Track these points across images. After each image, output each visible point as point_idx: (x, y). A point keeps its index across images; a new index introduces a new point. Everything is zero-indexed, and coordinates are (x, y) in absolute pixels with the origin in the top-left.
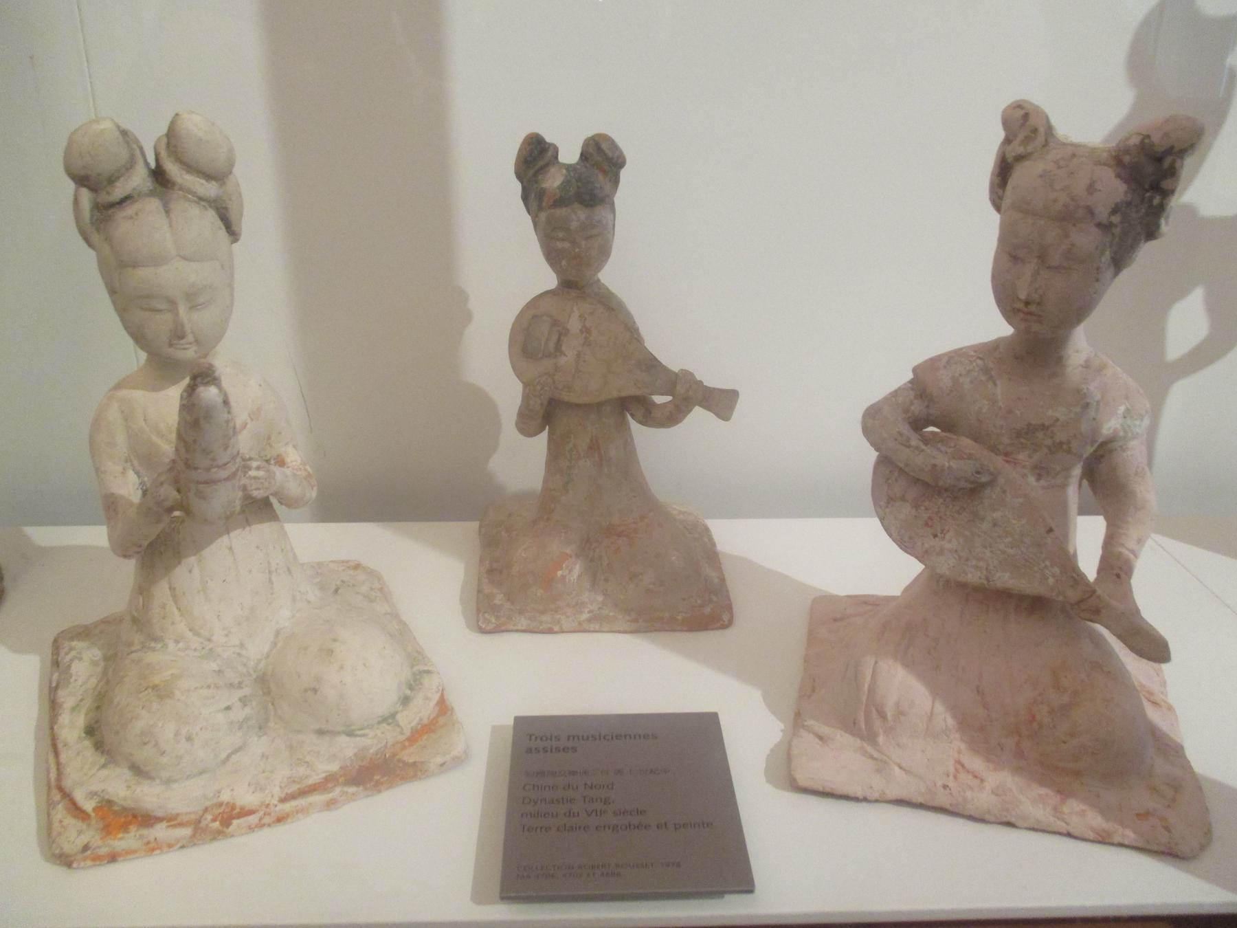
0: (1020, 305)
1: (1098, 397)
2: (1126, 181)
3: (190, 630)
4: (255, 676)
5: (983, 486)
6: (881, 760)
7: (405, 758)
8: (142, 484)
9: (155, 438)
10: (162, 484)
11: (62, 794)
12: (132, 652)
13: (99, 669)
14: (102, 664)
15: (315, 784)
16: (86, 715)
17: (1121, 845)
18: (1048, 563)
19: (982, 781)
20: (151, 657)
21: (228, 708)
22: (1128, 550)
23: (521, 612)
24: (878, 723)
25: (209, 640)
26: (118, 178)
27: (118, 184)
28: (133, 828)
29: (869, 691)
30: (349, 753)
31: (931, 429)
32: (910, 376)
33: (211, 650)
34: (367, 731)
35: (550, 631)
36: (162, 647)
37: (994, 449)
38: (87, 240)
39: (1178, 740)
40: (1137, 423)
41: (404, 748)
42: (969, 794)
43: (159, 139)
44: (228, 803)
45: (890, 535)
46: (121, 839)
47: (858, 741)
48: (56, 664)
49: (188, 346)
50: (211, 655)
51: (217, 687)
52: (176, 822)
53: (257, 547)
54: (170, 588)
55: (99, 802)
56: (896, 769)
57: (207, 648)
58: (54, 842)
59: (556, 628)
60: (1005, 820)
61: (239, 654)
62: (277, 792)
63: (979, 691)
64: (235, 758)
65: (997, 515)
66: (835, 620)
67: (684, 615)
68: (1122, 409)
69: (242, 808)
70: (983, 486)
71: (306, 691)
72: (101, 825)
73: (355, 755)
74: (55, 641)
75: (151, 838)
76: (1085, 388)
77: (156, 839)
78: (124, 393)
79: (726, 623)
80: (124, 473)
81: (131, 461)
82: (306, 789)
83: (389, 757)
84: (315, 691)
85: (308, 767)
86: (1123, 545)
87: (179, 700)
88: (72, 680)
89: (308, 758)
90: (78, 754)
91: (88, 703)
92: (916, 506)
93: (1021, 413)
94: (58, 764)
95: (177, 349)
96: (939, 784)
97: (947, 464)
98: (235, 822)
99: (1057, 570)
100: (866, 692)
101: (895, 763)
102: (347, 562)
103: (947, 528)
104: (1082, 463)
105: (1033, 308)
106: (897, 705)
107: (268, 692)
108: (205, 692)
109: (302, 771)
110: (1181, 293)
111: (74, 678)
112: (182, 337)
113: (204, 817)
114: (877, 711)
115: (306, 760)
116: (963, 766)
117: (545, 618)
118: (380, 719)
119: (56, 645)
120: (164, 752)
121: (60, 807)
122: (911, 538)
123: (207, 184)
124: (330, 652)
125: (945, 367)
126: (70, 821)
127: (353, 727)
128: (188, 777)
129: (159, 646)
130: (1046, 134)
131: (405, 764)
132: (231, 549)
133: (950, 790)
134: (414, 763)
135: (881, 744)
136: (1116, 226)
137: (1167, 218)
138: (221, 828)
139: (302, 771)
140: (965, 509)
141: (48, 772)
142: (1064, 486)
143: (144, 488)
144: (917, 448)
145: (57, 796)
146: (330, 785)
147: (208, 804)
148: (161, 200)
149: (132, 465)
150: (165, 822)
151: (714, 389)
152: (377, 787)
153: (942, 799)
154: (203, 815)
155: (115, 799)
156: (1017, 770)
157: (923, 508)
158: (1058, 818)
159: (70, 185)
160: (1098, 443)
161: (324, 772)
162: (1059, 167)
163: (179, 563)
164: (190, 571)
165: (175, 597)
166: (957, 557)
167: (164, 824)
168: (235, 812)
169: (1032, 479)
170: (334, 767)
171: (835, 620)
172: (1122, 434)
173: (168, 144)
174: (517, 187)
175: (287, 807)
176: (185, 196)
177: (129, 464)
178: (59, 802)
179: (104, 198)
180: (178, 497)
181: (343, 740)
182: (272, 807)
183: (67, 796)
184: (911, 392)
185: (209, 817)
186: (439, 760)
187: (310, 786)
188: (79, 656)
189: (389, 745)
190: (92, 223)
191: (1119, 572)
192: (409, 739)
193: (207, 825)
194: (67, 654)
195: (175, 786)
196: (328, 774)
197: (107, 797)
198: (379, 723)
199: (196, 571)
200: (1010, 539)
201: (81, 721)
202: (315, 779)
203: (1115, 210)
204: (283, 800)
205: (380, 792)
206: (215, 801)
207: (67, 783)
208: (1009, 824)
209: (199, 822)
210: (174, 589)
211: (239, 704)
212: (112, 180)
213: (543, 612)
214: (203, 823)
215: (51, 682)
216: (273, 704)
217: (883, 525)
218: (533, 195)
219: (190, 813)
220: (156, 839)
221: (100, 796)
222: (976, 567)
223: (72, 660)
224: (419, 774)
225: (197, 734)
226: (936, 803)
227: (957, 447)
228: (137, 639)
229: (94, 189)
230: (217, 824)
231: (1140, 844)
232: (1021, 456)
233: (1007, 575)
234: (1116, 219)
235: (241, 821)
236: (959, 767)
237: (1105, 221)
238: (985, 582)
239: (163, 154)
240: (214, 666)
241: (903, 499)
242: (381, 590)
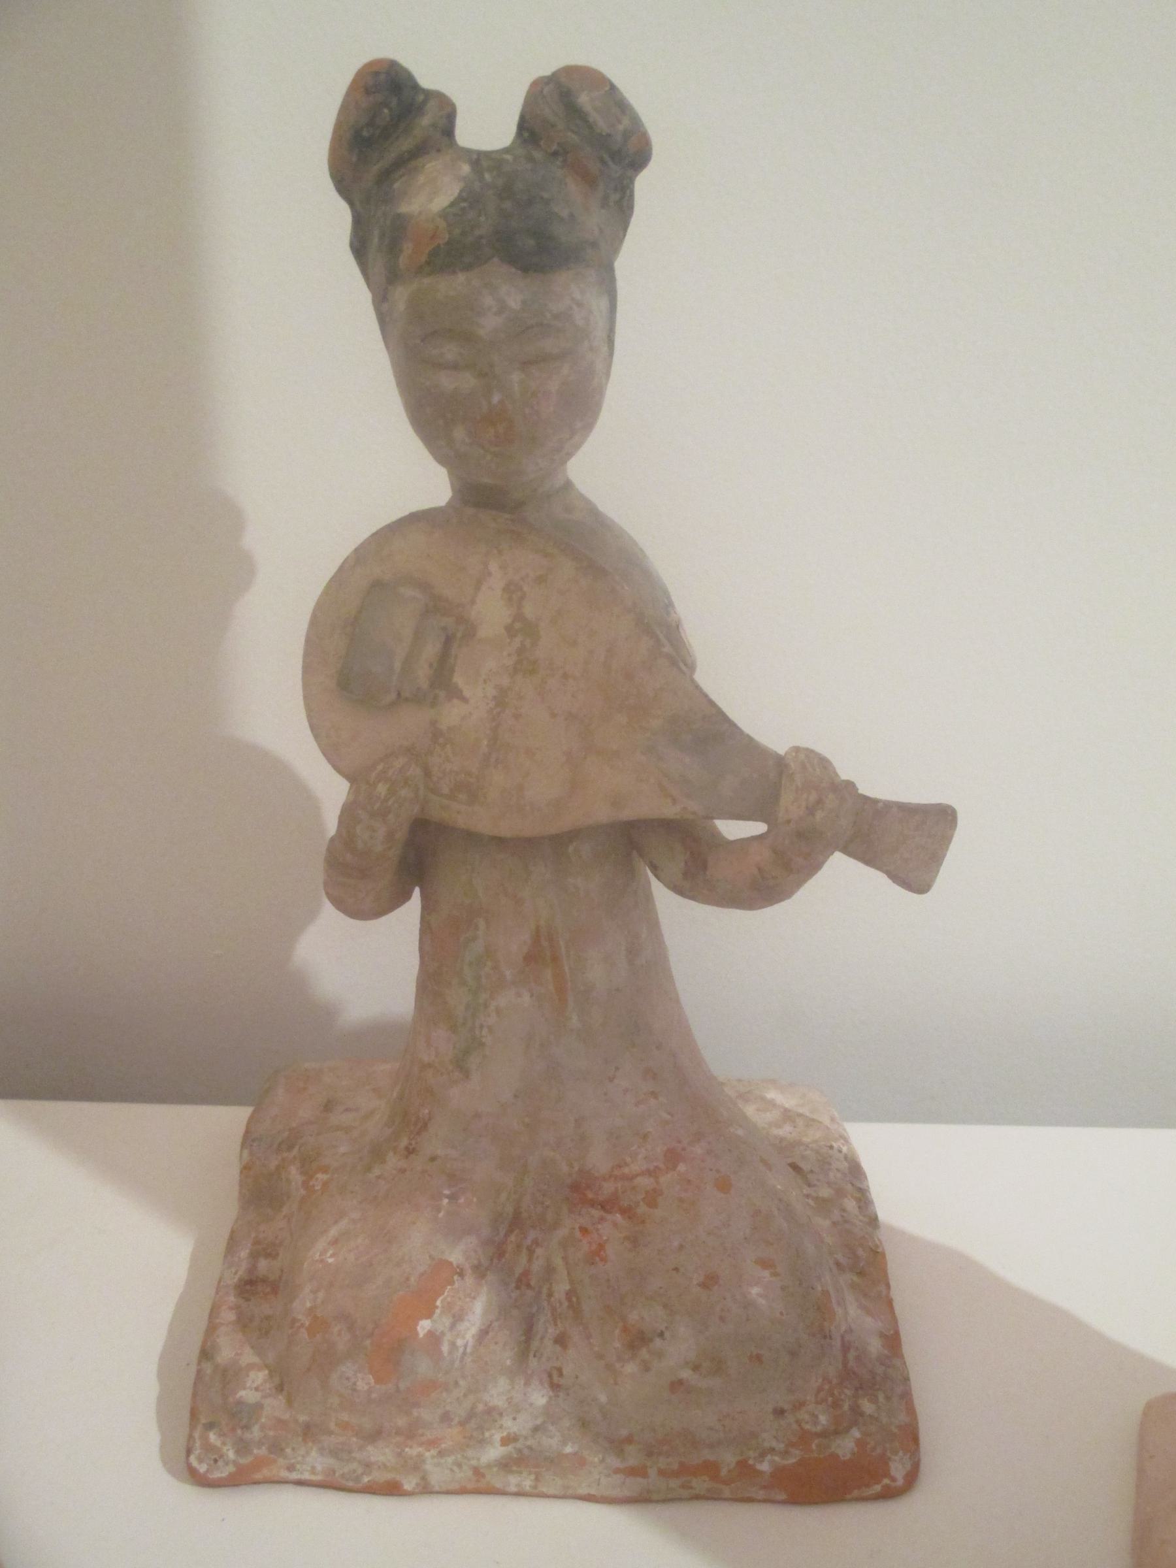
35: (392, 1489)
79: (900, 1482)
151: (889, 805)
213: (375, 1436)
231: (626, 1493)
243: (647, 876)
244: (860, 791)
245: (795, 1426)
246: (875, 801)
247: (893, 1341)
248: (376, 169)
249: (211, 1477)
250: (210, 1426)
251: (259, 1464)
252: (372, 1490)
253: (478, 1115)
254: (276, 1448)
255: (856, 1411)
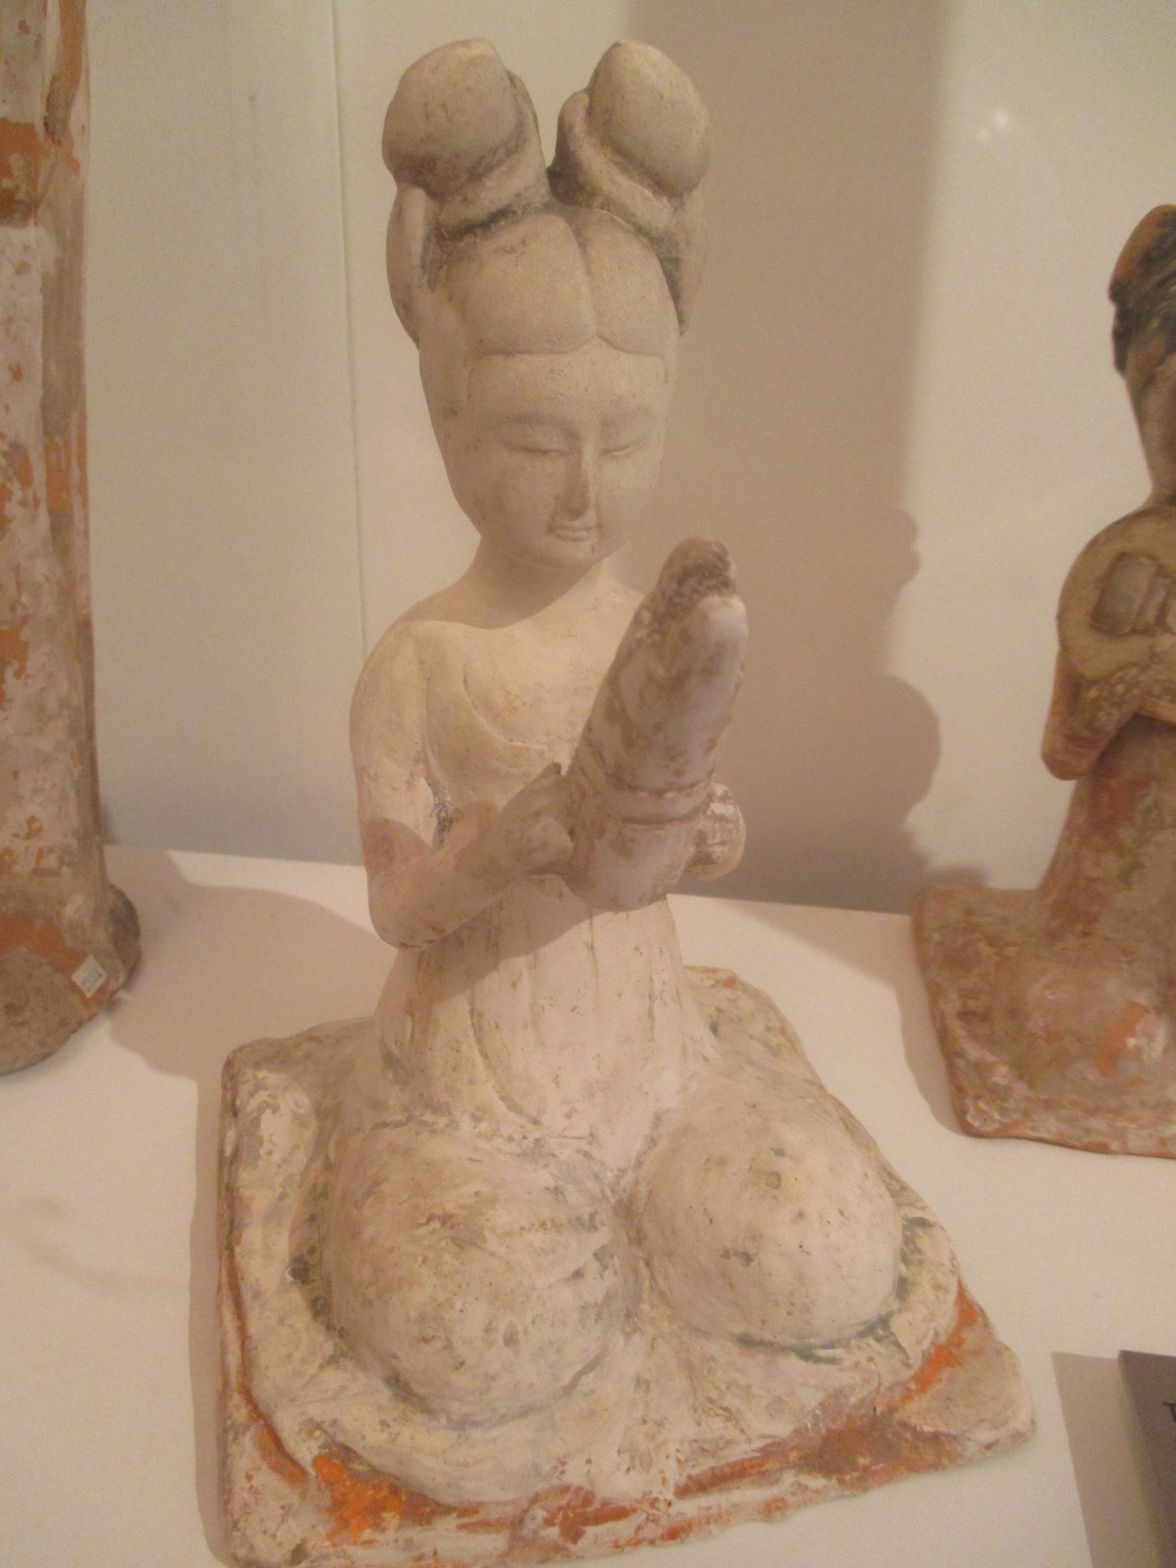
3: (502, 1098)
4: (613, 1200)
7: (914, 1421)
8: (441, 805)
9: (482, 721)
10: (537, 814)
11: (250, 1407)
12: (385, 1125)
13: (309, 1134)
14: (313, 1124)
15: (742, 1462)
16: (292, 1232)
20: (434, 1148)
21: (578, 1274)
23: (1049, 1105)
25: (536, 1122)
26: (490, 168)
27: (488, 182)
28: (391, 1518)
30: (811, 1399)
33: (537, 1141)
34: (838, 1352)
35: (1101, 1149)
36: (447, 1126)
38: (405, 308)
41: (907, 1397)
43: (573, 98)
44: (579, 1489)
46: (369, 1543)
48: (232, 1110)
49: (584, 534)
50: (537, 1152)
51: (558, 1227)
52: (474, 1519)
53: (637, 949)
54: (472, 1013)
55: (323, 1447)
57: (531, 1138)
58: (235, 1524)
59: (1115, 1145)
61: (587, 1155)
62: (676, 1476)
64: (588, 1381)
69: (605, 1503)
71: (726, 1254)
72: (327, 1501)
73: (822, 1405)
74: (229, 1064)
75: (427, 1550)
77: (435, 1553)
78: (429, 626)
80: (410, 784)
81: (426, 761)
82: (727, 1470)
83: (882, 1412)
84: (747, 1258)
85: (728, 1419)
87: (492, 1254)
88: (263, 1151)
89: (730, 1401)
90: (281, 1321)
91: (294, 1206)
94: (242, 1331)
95: (559, 537)
98: (590, 1531)
102: (715, 971)
107: (639, 1239)
108: (538, 1238)
109: (717, 1427)
111: (266, 1146)
112: (577, 513)
113: (530, 1514)
115: (725, 1404)
117: (1097, 1123)
118: (862, 1328)
119: (231, 1073)
120: (462, 1364)
121: (247, 1440)
123: (654, 199)
124: (775, 1180)
126: (266, 1478)
127: (812, 1341)
128: (503, 1420)
129: (442, 1122)
131: (918, 1435)
132: (591, 947)
134: (936, 1438)
138: (561, 1542)
139: (717, 1427)
141: (224, 1353)
143: (443, 814)
145: (241, 1413)
146: (770, 1465)
147: (541, 1486)
148: (570, 222)
149: (428, 768)
150: (454, 1515)
152: (863, 1481)
154: (530, 1507)
155: (358, 1447)
159: (387, 186)
161: (763, 1436)
163: (496, 966)
164: (514, 985)
165: (479, 1031)
167: (452, 1521)
168: (590, 1509)
170: (782, 1429)
173: (590, 112)
174: (1106, 314)
175: (690, 1507)
176: (613, 220)
177: (421, 766)
178: (247, 1428)
179: (457, 212)
180: (568, 843)
181: (792, 1364)
182: (662, 1505)
183: (261, 1417)
185: (540, 1514)
186: (985, 1435)
187: (732, 1465)
188: (271, 1101)
189: (882, 1389)
190: (423, 266)
192: (916, 1378)
193: (535, 1532)
194: (252, 1095)
195: (476, 1435)
196: (769, 1441)
197: (340, 1438)
198: (861, 1335)
199: (525, 984)
201: (283, 1245)
202: (741, 1451)
204: (683, 1492)
205: (865, 1490)
206: (556, 1482)
207: (264, 1389)
209: (521, 1522)
210: (480, 1015)
211: (595, 1265)
212: (478, 173)
213: (1093, 1112)
214: (526, 1532)
215: (222, 1151)
216: (648, 1264)
218: (1155, 323)
219: (506, 1503)
220: (435, 1553)
221: (326, 1433)
223: (261, 1109)
224: (945, 1460)
225: (526, 1332)
228: (394, 1096)
229: (436, 194)
230: (554, 1532)
235: (603, 1529)
239: (579, 126)
240: (545, 1178)
242: (783, 1031)
248: (1157, 278)
249: (982, 1129)
250: (977, 1097)
251: (1016, 1124)
252: (1088, 1148)
253: (1135, 913)
254: (1026, 1114)
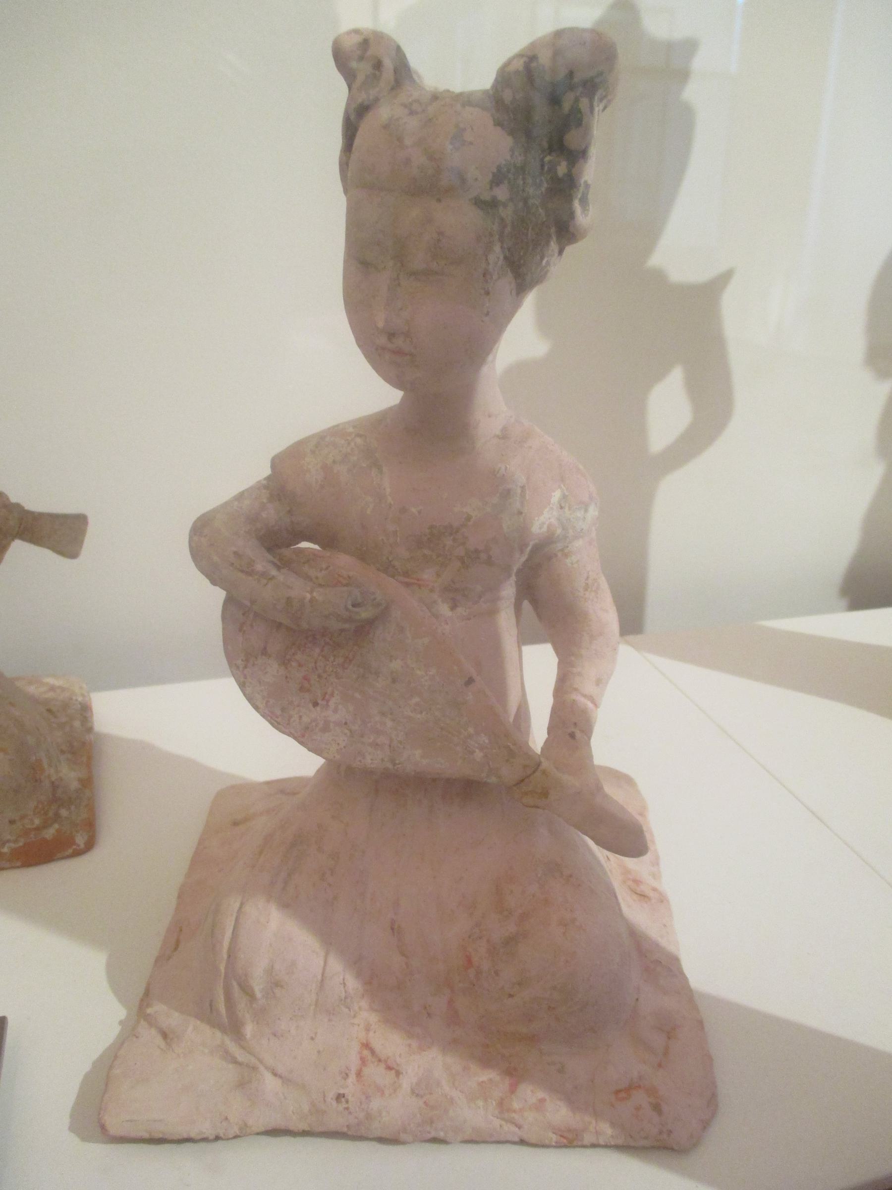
0: (382, 340)
1: (522, 479)
2: (512, 133)
5: (371, 623)
6: (248, 1066)
17: (594, 1146)
18: (471, 730)
19: (398, 1074)
22: (585, 696)
24: (242, 1004)
29: (229, 956)
31: (304, 545)
32: (266, 471)
37: (388, 569)
39: (671, 948)
40: (579, 514)
42: (376, 1104)
45: (256, 708)
47: (218, 1034)
56: (268, 1077)
60: (429, 1136)
63: (394, 929)
65: (396, 665)
66: (236, 824)
67: (13, 845)
68: (557, 495)
70: (371, 623)
76: (503, 468)
79: (82, 846)
86: (576, 689)
92: (285, 662)
93: (420, 512)
96: (331, 1095)
97: (308, 596)
99: (484, 739)
100: (225, 956)
101: (267, 1068)
103: (330, 690)
104: (513, 578)
105: (399, 342)
106: (270, 971)
110: (660, 375)
114: (240, 985)
116: (373, 1052)
122: (283, 710)
125: (313, 452)
130: (396, 71)
133: (347, 1102)
135: (248, 1036)
136: (505, 205)
137: (584, 202)
140: (351, 661)
142: (492, 613)
144: (264, 574)
151: (41, 515)
153: (336, 1120)
156: (452, 1045)
157: (294, 664)
158: (503, 1119)
160: (529, 548)
162: (412, 113)
166: (349, 734)
169: (444, 609)
171: (236, 824)
172: (559, 531)
184: (264, 491)
191: (573, 730)
200: (416, 699)
203: (497, 179)
208: (435, 1140)
217: (245, 694)
222: (375, 745)
226: (332, 1127)
227: (331, 568)
231: (620, 1142)
232: (428, 575)
233: (418, 753)
234: (502, 193)
236: (366, 1053)
237: (486, 196)
238: (390, 766)
241: (264, 652)
243: (587, 845)
244: (547, 736)
245: (21, 827)
246: (32, 513)
247: (87, 782)
255: (57, 815)
